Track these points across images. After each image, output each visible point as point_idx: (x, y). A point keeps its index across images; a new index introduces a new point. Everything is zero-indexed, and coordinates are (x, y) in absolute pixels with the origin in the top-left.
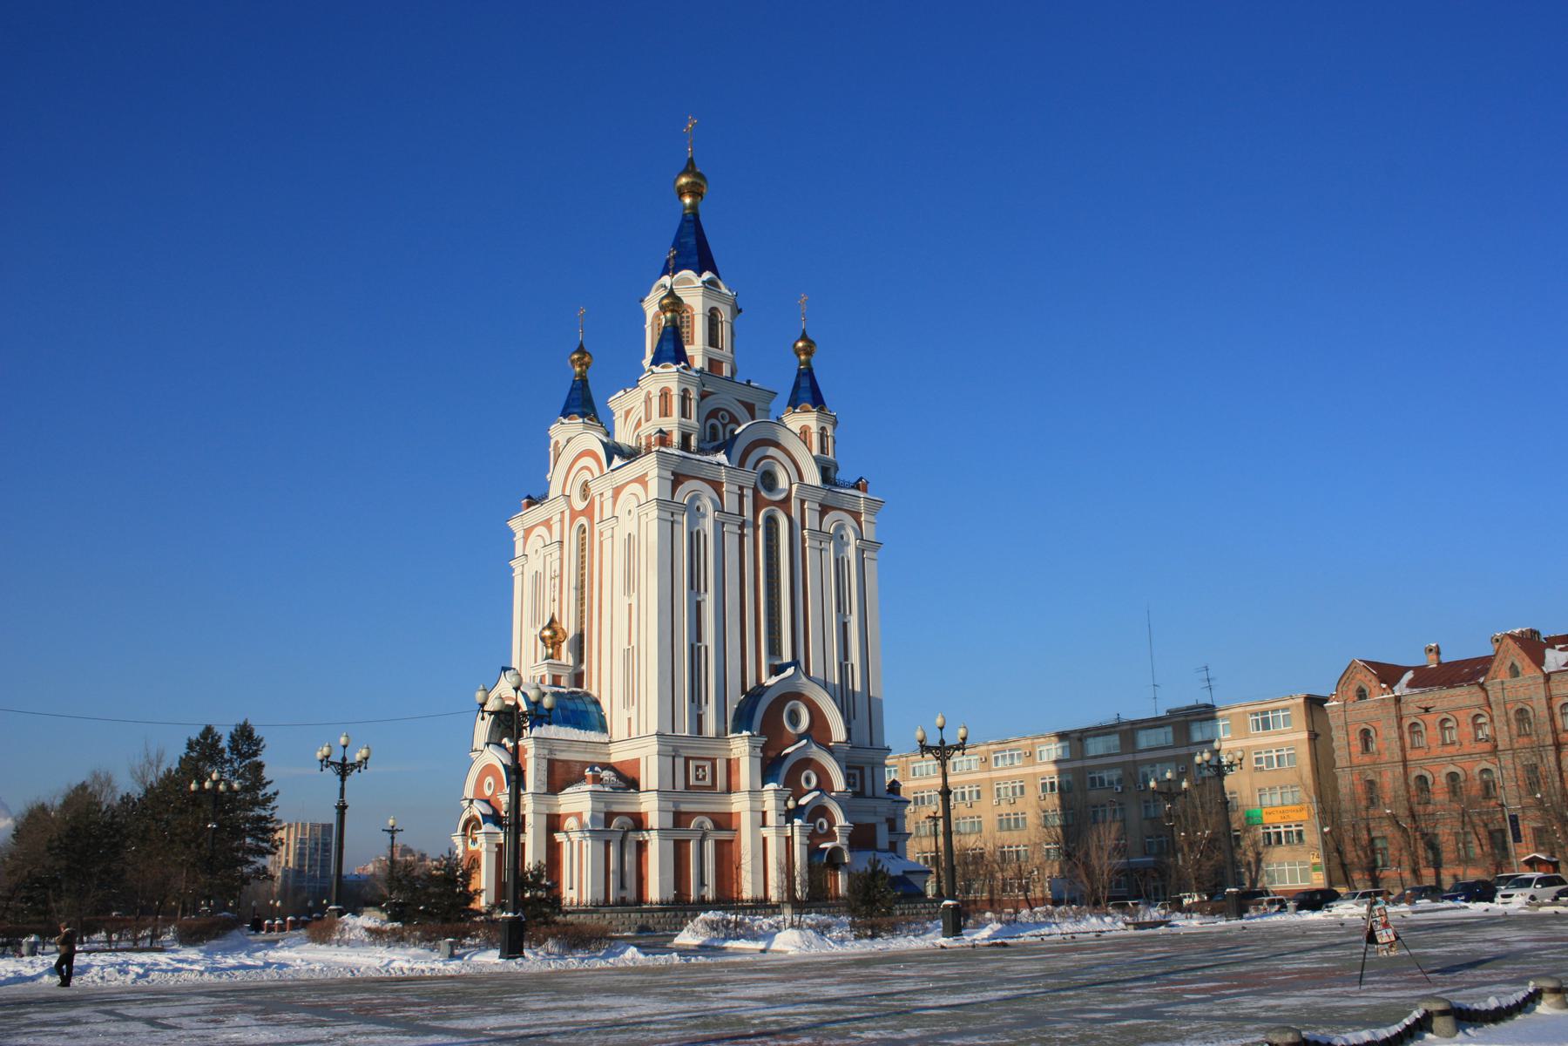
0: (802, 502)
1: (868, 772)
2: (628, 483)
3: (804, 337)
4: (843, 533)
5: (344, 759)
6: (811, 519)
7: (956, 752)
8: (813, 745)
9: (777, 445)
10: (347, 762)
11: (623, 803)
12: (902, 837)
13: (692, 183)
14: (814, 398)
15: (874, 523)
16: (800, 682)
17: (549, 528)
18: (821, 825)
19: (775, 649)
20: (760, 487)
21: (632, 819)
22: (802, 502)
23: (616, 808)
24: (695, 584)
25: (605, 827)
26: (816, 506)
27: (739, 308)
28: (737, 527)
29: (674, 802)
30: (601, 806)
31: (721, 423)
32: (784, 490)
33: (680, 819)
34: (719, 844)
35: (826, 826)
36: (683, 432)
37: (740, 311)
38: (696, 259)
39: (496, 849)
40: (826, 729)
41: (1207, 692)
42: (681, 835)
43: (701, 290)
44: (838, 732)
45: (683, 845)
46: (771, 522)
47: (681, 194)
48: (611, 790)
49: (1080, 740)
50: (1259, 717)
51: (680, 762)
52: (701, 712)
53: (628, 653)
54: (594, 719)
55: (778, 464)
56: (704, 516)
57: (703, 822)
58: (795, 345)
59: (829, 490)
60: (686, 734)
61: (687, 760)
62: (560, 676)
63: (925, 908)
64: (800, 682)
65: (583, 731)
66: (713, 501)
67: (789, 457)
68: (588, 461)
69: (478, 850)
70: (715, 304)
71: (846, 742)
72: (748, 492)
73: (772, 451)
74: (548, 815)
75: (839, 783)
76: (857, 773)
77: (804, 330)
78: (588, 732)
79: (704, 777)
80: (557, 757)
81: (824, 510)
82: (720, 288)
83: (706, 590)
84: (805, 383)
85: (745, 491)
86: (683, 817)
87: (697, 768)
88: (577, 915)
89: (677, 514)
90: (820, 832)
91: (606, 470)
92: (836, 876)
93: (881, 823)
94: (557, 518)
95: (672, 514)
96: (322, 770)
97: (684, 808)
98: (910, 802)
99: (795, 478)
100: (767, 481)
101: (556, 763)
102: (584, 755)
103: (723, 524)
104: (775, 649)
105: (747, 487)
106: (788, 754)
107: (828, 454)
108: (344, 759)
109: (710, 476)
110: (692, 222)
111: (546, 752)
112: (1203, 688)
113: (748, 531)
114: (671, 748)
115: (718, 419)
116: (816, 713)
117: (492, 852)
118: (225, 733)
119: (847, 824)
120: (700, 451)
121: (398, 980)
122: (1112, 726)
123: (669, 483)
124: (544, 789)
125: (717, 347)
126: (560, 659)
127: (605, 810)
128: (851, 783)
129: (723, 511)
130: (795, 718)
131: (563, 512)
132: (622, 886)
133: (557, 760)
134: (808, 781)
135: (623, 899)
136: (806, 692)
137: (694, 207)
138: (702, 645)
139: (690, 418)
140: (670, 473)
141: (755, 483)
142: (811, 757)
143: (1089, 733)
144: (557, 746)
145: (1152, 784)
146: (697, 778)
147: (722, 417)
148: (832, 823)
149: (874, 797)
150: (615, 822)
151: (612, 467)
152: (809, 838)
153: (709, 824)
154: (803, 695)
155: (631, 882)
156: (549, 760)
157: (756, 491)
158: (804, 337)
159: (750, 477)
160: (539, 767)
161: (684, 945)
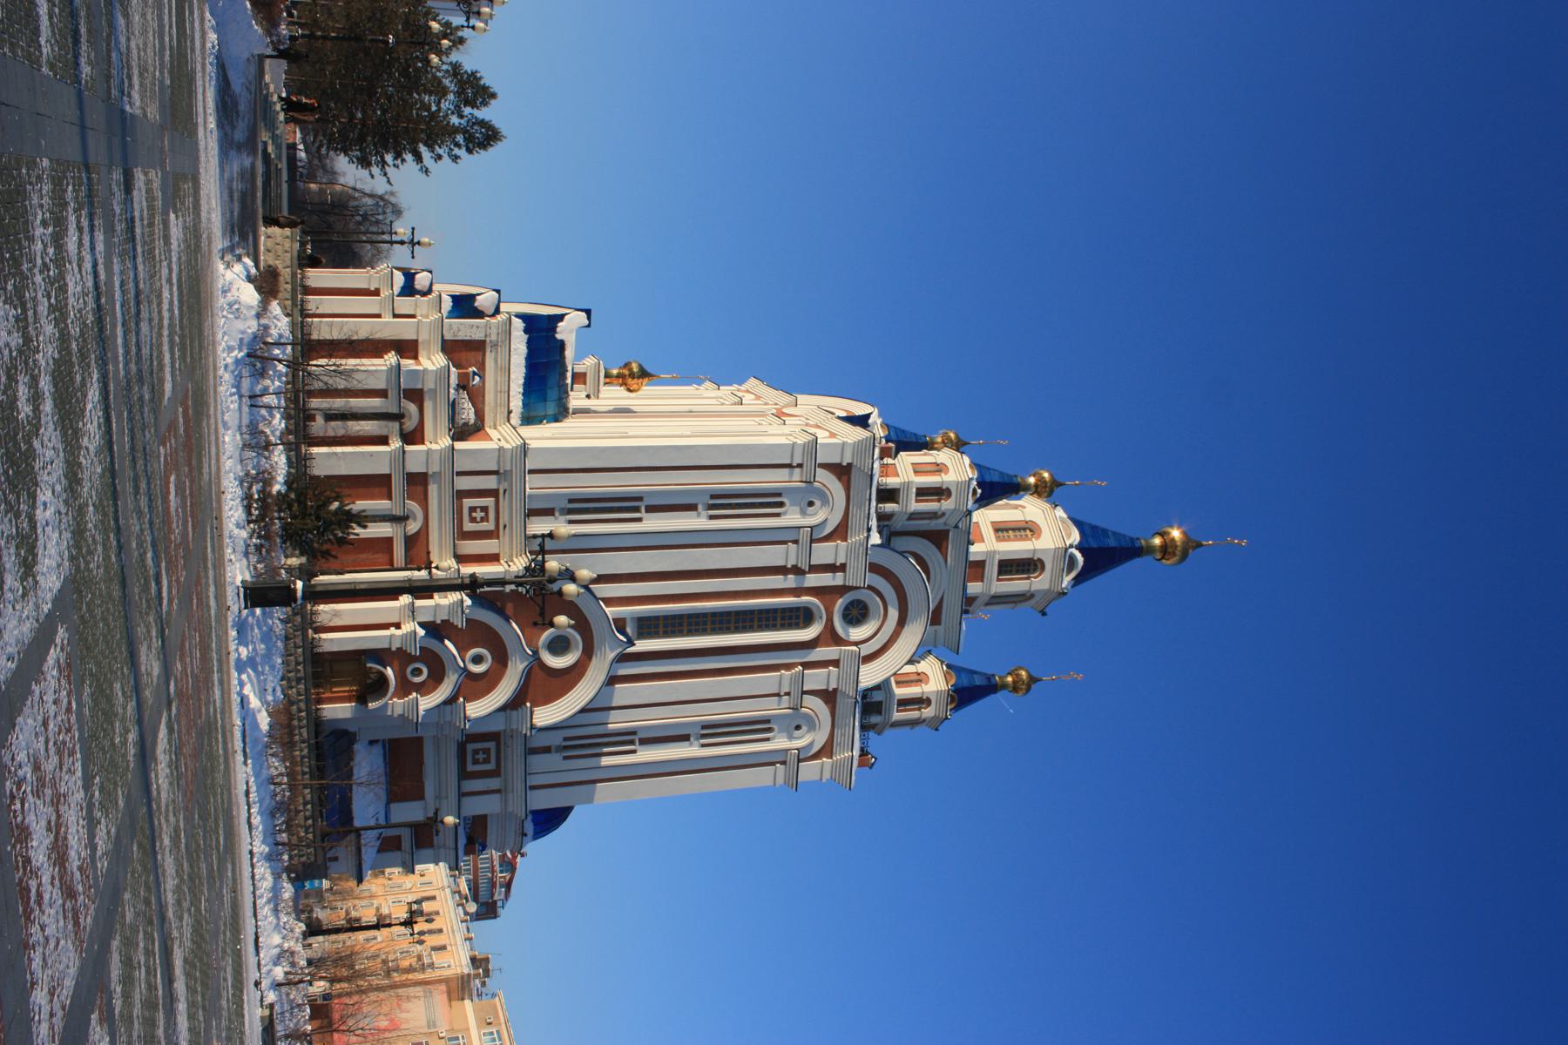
0: (836, 663)
1: (493, 783)
3: (1033, 680)
4: (804, 728)
8: (526, 664)
9: (902, 623)
11: (435, 417)
12: (408, 857)
13: (1176, 547)
16: (608, 650)
18: (417, 672)
19: (649, 626)
20: (849, 597)
21: (415, 430)
22: (836, 663)
23: (428, 405)
24: (721, 502)
25: (404, 390)
27: (1046, 610)
29: (440, 473)
30: (429, 385)
32: (848, 634)
33: (417, 483)
34: (387, 542)
35: (417, 680)
39: (372, 289)
42: (397, 485)
43: (1061, 545)
44: (546, 715)
45: (385, 490)
46: (801, 617)
47: (1162, 534)
48: (451, 399)
51: (490, 483)
52: (557, 514)
55: (879, 623)
56: (791, 738)
57: (415, 519)
58: (1021, 668)
59: (856, 702)
60: (528, 490)
61: (493, 493)
62: (585, 383)
63: (305, 804)
64: (608, 650)
65: (521, 390)
66: (811, 744)
67: (888, 641)
70: (1048, 566)
71: (532, 727)
72: (837, 580)
73: (893, 614)
74: (416, 341)
75: (477, 709)
77: (1040, 680)
78: (521, 397)
79: (473, 520)
80: (488, 353)
81: (829, 696)
82: (1067, 575)
83: (703, 746)
85: (840, 575)
86: (420, 489)
87: (485, 509)
88: (289, 280)
89: (802, 472)
90: (409, 669)
92: (349, 699)
93: (425, 809)
95: (788, 694)
97: (433, 489)
99: (866, 649)
100: (855, 612)
101: (481, 353)
102: (492, 391)
103: (784, 763)
104: (649, 626)
105: (845, 576)
106: (510, 624)
107: (898, 711)
109: (852, 521)
110: (1131, 551)
111: (494, 337)
113: (791, 581)
114: (509, 468)
116: (567, 679)
117: (369, 284)
118: (489, 21)
119: (421, 713)
120: (882, 517)
123: (836, 460)
124: (448, 337)
125: (1000, 573)
126: (605, 384)
127: (425, 389)
128: (483, 514)
129: (812, 541)
130: (559, 645)
132: (330, 417)
133: (484, 355)
134: (478, 660)
136: (594, 661)
138: (642, 514)
140: (850, 461)
142: (510, 663)
144: (502, 351)
146: (472, 509)
148: (423, 689)
149: (462, 795)
150: (412, 408)
152: (399, 649)
153: (413, 527)
154: (590, 659)
155: (337, 428)
156: (483, 342)
157: (843, 590)
158: (1033, 680)
159: (857, 575)
160: (475, 328)
161: (240, 862)
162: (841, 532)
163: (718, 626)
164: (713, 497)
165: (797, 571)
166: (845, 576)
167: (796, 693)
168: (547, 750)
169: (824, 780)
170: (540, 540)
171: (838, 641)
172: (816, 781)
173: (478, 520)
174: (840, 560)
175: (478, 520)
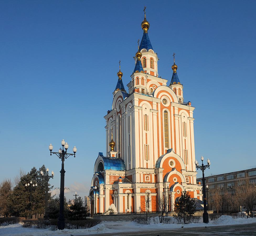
2: (128, 103)
5: (203, 165)
6: (176, 112)
19: (167, 146)
26: (177, 108)
49: (247, 172)
53: (147, 129)
68: (120, 99)
72: (159, 105)
94: (114, 115)
96: (198, 169)
99: (172, 101)
108: (203, 165)
121: (121, 215)
131: (115, 113)
143: (249, 171)
162: (151, 103)
165: (158, 113)
168: (147, 164)
174: (156, 103)
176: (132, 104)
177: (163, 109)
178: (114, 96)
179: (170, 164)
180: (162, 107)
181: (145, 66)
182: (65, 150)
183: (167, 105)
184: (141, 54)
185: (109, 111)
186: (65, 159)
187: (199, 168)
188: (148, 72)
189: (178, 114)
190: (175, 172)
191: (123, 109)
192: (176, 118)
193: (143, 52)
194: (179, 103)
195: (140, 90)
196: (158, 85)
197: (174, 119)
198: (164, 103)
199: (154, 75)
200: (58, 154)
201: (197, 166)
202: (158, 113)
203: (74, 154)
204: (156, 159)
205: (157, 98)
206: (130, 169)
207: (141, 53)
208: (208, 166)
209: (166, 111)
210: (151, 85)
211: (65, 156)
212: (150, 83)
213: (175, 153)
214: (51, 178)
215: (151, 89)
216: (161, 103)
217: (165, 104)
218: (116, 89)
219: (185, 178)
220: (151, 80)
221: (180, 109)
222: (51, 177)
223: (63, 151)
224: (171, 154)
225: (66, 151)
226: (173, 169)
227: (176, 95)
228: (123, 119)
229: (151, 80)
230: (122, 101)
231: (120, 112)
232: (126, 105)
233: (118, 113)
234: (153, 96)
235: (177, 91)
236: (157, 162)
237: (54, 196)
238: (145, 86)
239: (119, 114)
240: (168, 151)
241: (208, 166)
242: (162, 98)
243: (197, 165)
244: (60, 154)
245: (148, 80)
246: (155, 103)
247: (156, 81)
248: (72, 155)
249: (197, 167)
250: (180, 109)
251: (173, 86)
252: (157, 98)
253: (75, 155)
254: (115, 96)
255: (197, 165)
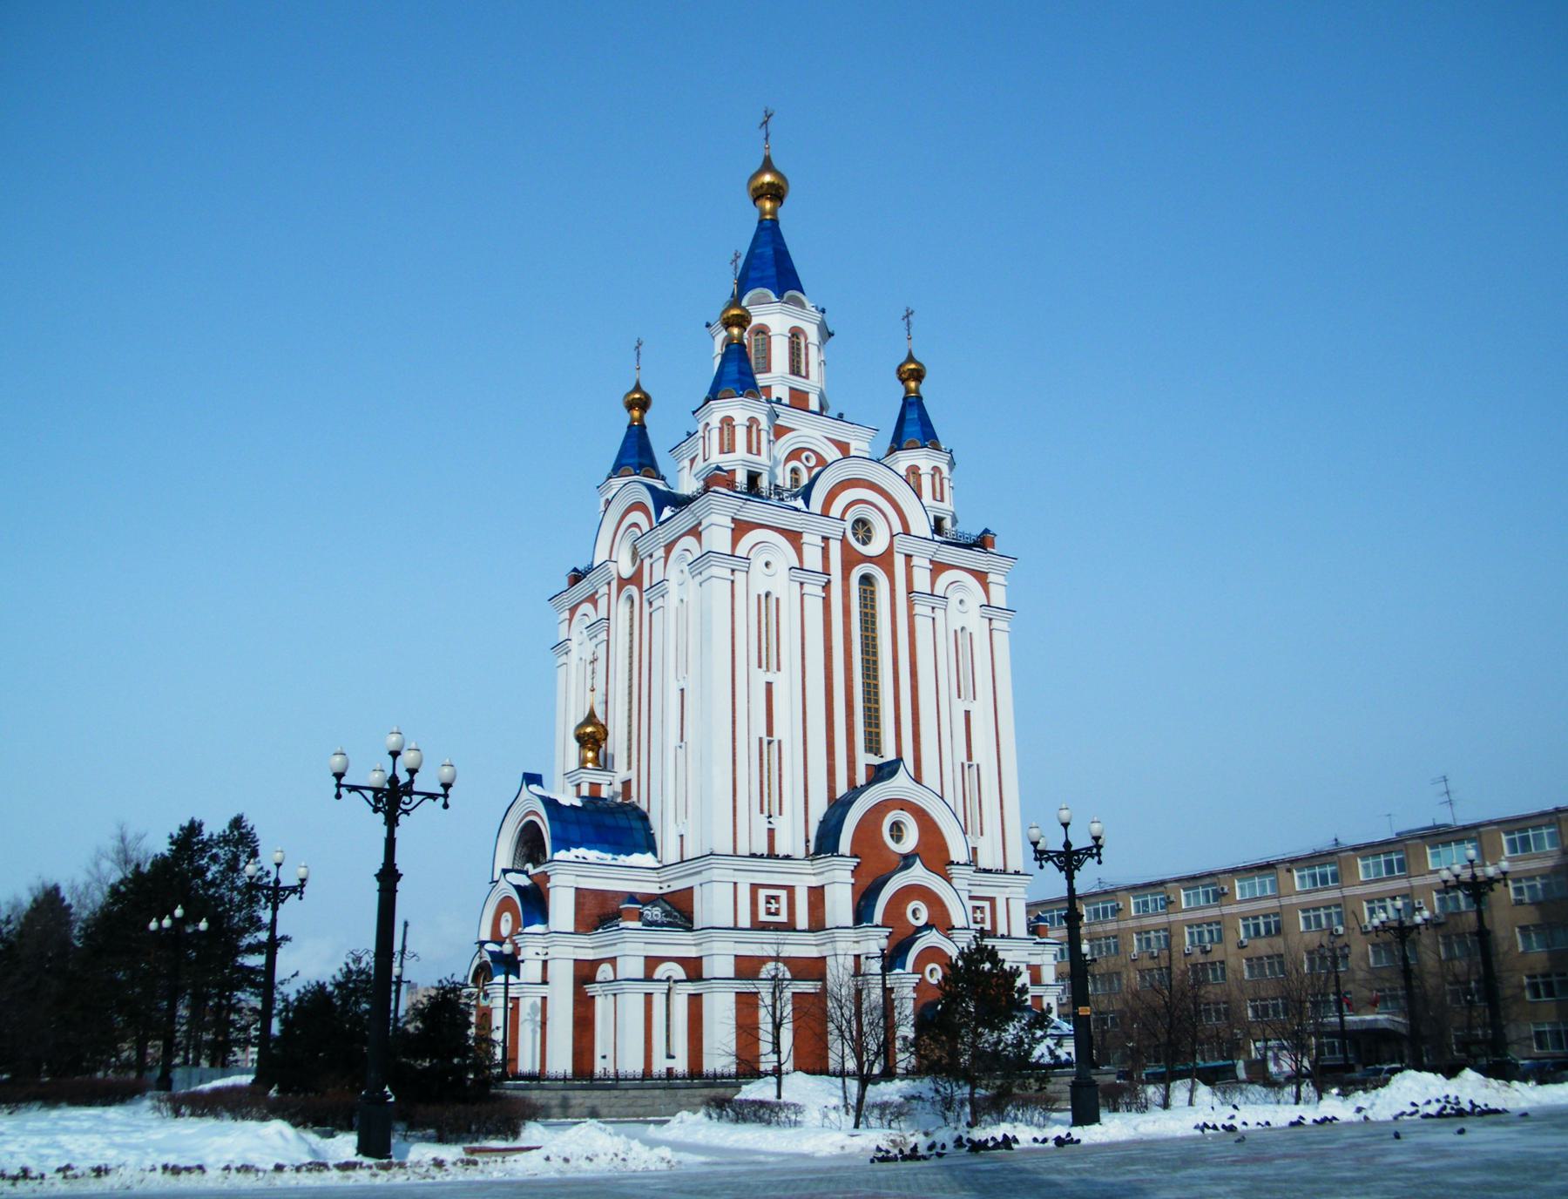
2: (680, 537)
5: (1067, 844)
6: (922, 580)
7: (293, 895)
10: (281, 885)
14: (924, 433)
15: (1005, 586)
17: (595, 603)
19: (873, 745)
26: (927, 563)
28: (821, 588)
31: (805, 466)
36: (749, 471)
37: (831, 335)
38: (772, 271)
40: (943, 847)
41: (1446, 808)
50: (1517, 836)
54: (640, 837)
68: (638, 516)
69: (488, 1006)
76: (986, 904)
84: (913, 415)
91: (655, 525)
96: (338, 796)
98: (518, 977)
99: (897, 528)
105: (833, 538)
108: (1067, 844)
112: (1441, 803)
115: (800, 461)
122: (1330, 854)
131: (609, 584)
135: (669, 1070)
137: (774, 212)
139: (759, 453)
140: (730, 519)
141: (844, 533)
145: (458, 1016)
147: (807, 459)
151: (662, 519)
162: (794, 538)
163: (871, 673)
164: (760, 666)
165: (826, 587)
166: (833, 538)
167: (734, 563)
169: (1006, 583)
170: (343, 791)
171: (889, 554)
172: (1006, 591)
173: (982, 916)
175: (982, 916)
176: (698, 545)
177: (857, 568)
178: (602, 501)
179: (892, 836)
180: (851, 559)
181: (767, 369)
182: (404, 778)
183: (876, 547)
184: (747, 311)
185: (575, 570)
186: (403, 818)
187: (1050, 859)
188: (780, 392)
189: (932, 590)
190: (918, 874)
191: (651, 565)
192: (918, 609)
193: (757, 302)
194: (933, 540)
195: (741, 478)
196: (831, 454)
197: (911, 617)
198: (858, 540)
199: (808, 405)
200: (369, 794)
201: (1042, 852)
202: (826, 587)
203: (441, 791)
204: (819, 808)
205: (825, 513)
206: (682, 856)
207: (744, 309)
208: (1095, 851)
209: (866, 580)
210: (795, 454)
211: (404, 803)
212: (785, 445)
213: (918, 779)
214: (294, 898)
215: (794, 471)
216: (844, 541)
217: (865, 543)
218: (618, 470)
219: (970, 904)
220: (792, 430)
221: (938, 568)
222: (294, 890)
223: (394, 779)
224: (899, 785)
225: (411, 782)
226: (907, 861)
227: (919, 497)
228: (651, 614)
229: (792, 430)
230: (646, 528)
231: (636, 579)
232: (669, 548)
233: (623, 582)
234: (807, 504)
235: (926, 482)
236: (822, 823)
237: (286, 982)
238: (763, 459)
239: (634, 590)
240: (881, 773)
241: (1095, 851)
242: (851, 516)
243: (1040, 847)
244: (376, 790)
245: (780, 432)
246: (811, 542)
247: (818, 434)
248: (433, 796)
249: (1041, 855)
250: (938, 568)
251: (904, 460)
252: (825, 513)
253: (446, 796)
254: (608, 502)
255: (1040, 847)
